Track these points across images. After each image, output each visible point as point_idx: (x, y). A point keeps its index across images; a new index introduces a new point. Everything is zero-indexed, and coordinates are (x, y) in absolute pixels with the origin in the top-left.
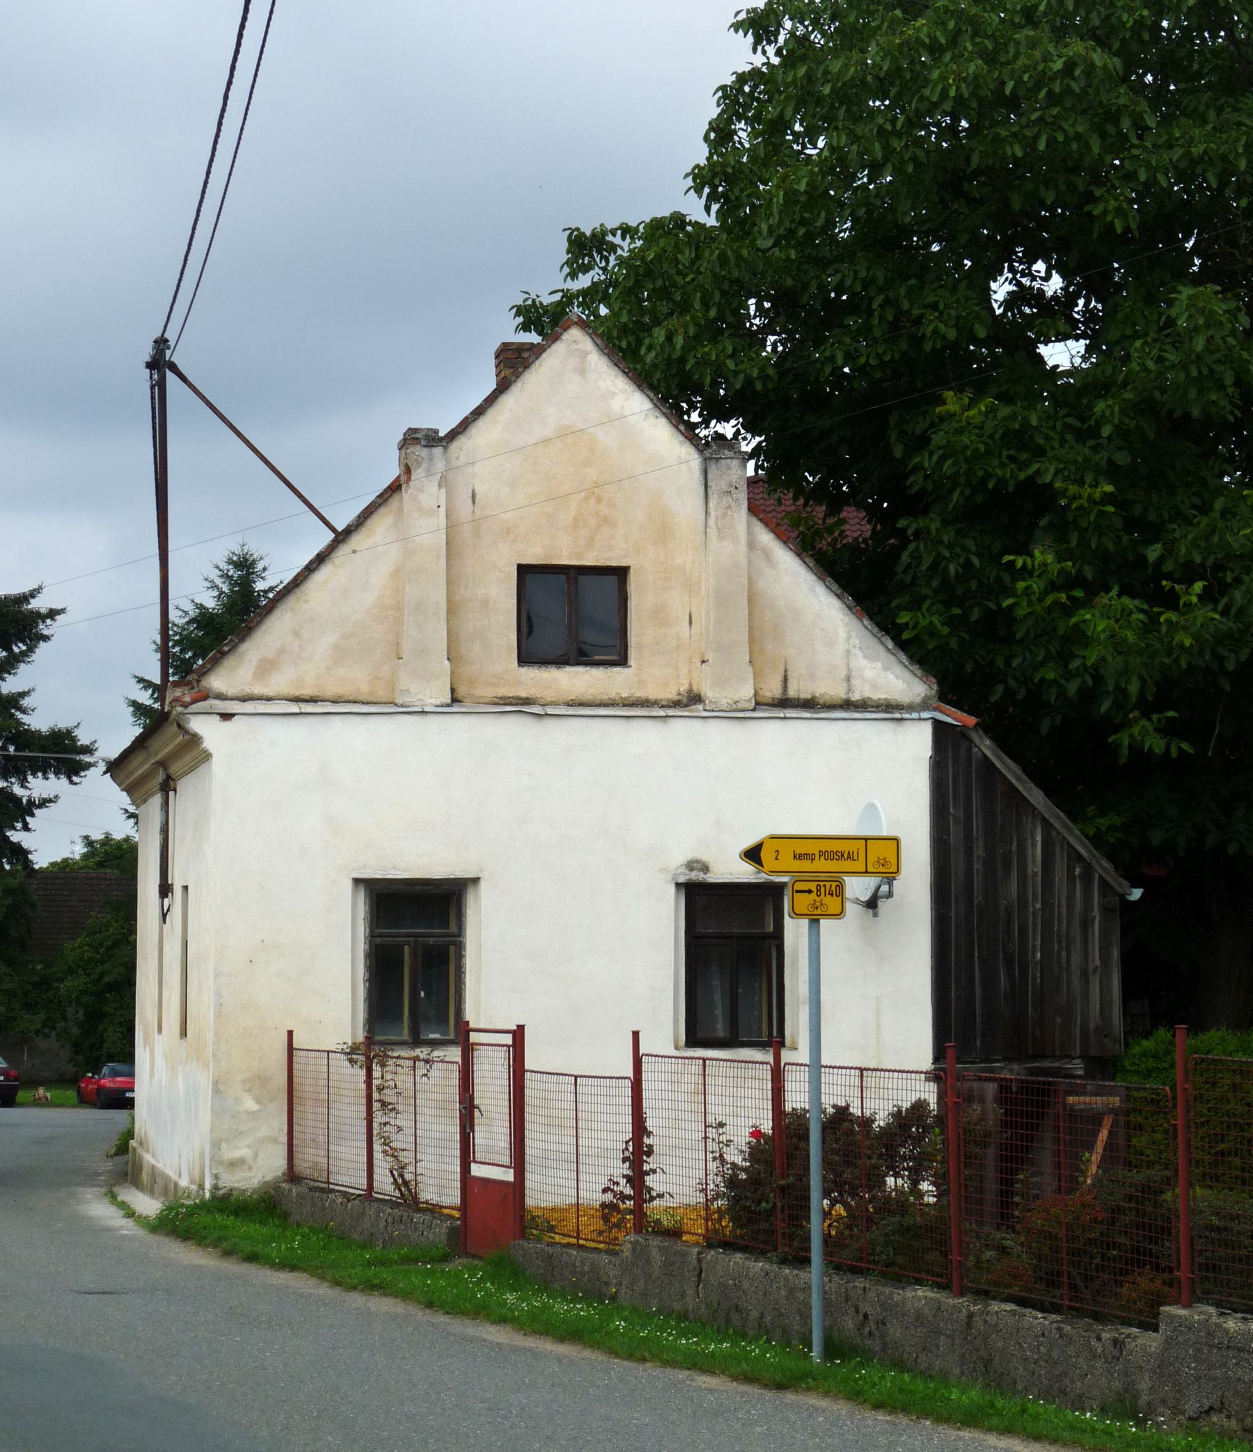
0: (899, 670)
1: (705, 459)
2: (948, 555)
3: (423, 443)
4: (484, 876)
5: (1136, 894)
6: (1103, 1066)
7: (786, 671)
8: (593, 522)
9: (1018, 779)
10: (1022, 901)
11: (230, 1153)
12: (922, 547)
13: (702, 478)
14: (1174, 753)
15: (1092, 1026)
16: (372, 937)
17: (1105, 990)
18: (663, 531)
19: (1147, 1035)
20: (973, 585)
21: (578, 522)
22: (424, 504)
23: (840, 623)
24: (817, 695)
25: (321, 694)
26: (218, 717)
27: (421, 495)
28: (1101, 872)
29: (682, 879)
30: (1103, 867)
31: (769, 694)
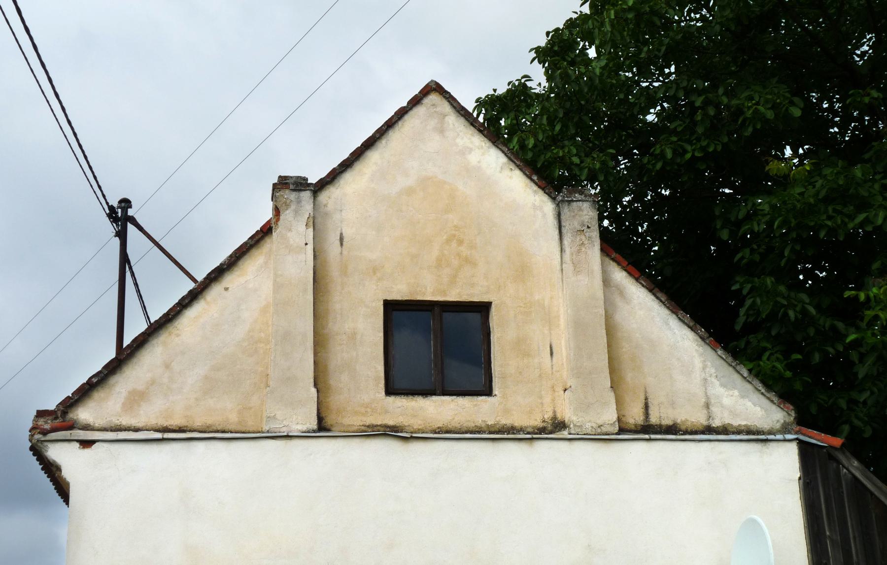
1: (558, 205)
2: (786, 303)
3: (292, 187)
7: (646, 399)
8: (455, 262)
12: (758, 301)
13: (556, 223)
18: (522, 270)
20: (812, 331)
21: (440, 263)
22: (292, 242)
23: (695, 354)
24: (679, 421)
26: (77, 445)
27: (289, 234)
31: (631, 421)
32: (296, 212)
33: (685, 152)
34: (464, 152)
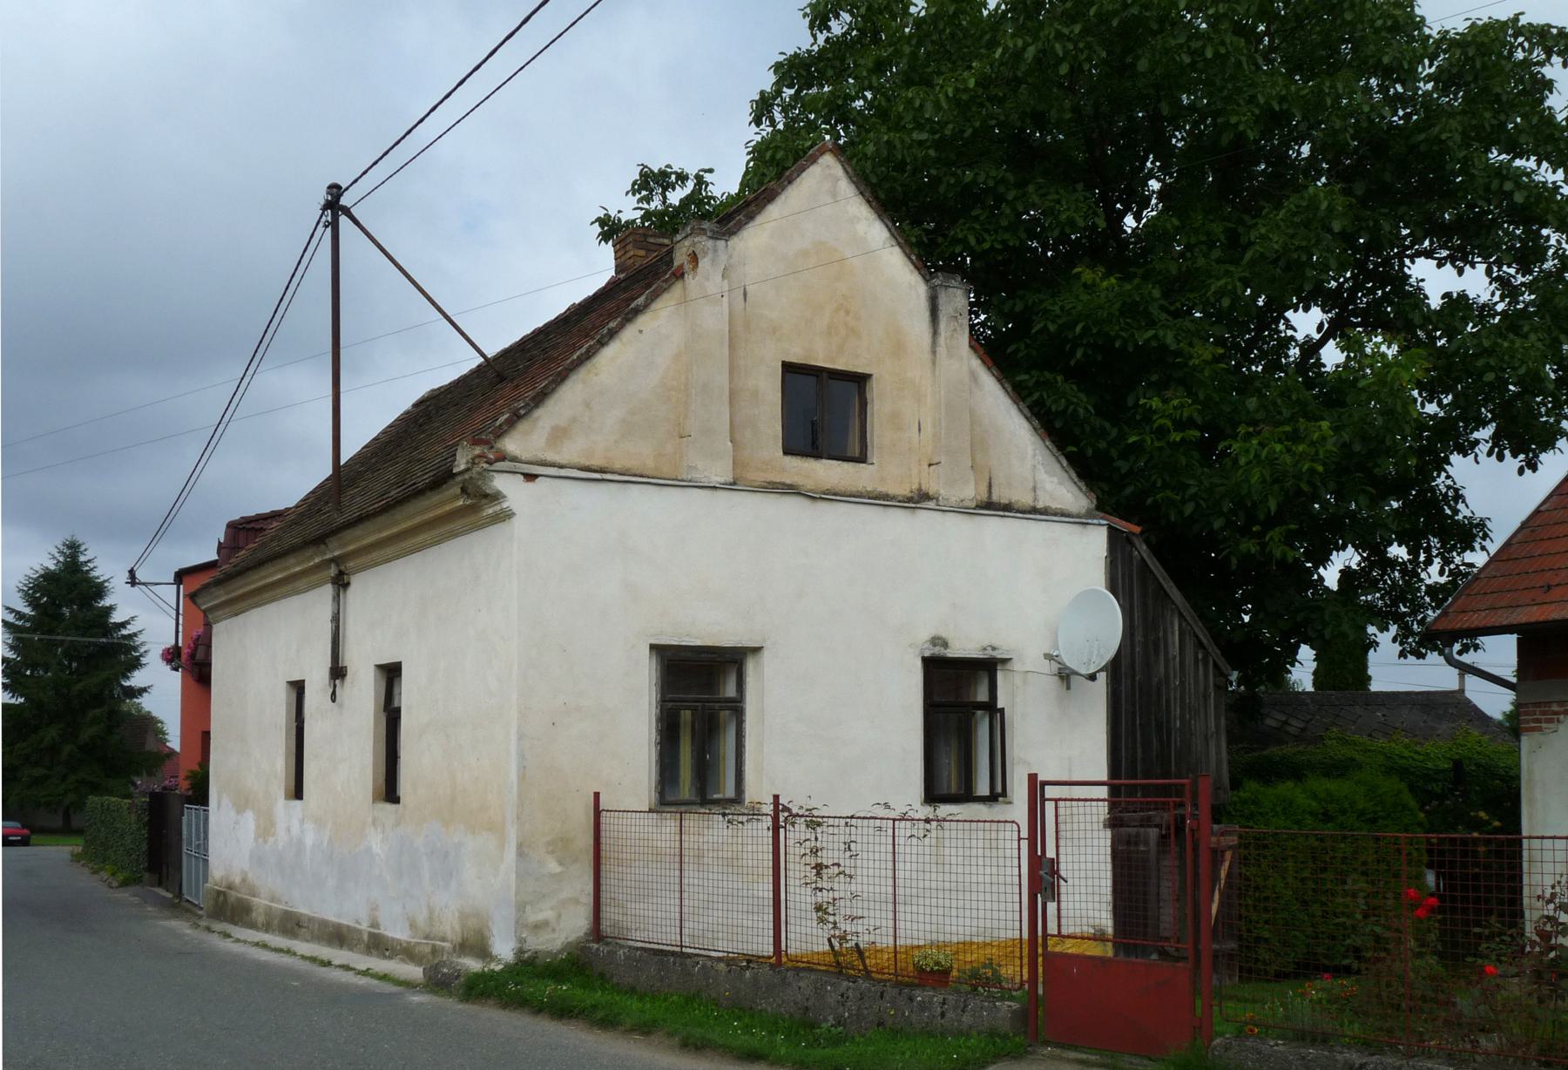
11: (534, 917)
16: (663, 701)
18: (898, 348)
29: (927, 654)
30: (1215, 652)
32: (713, 261)
33: (985, 240)
34: (861, 228)
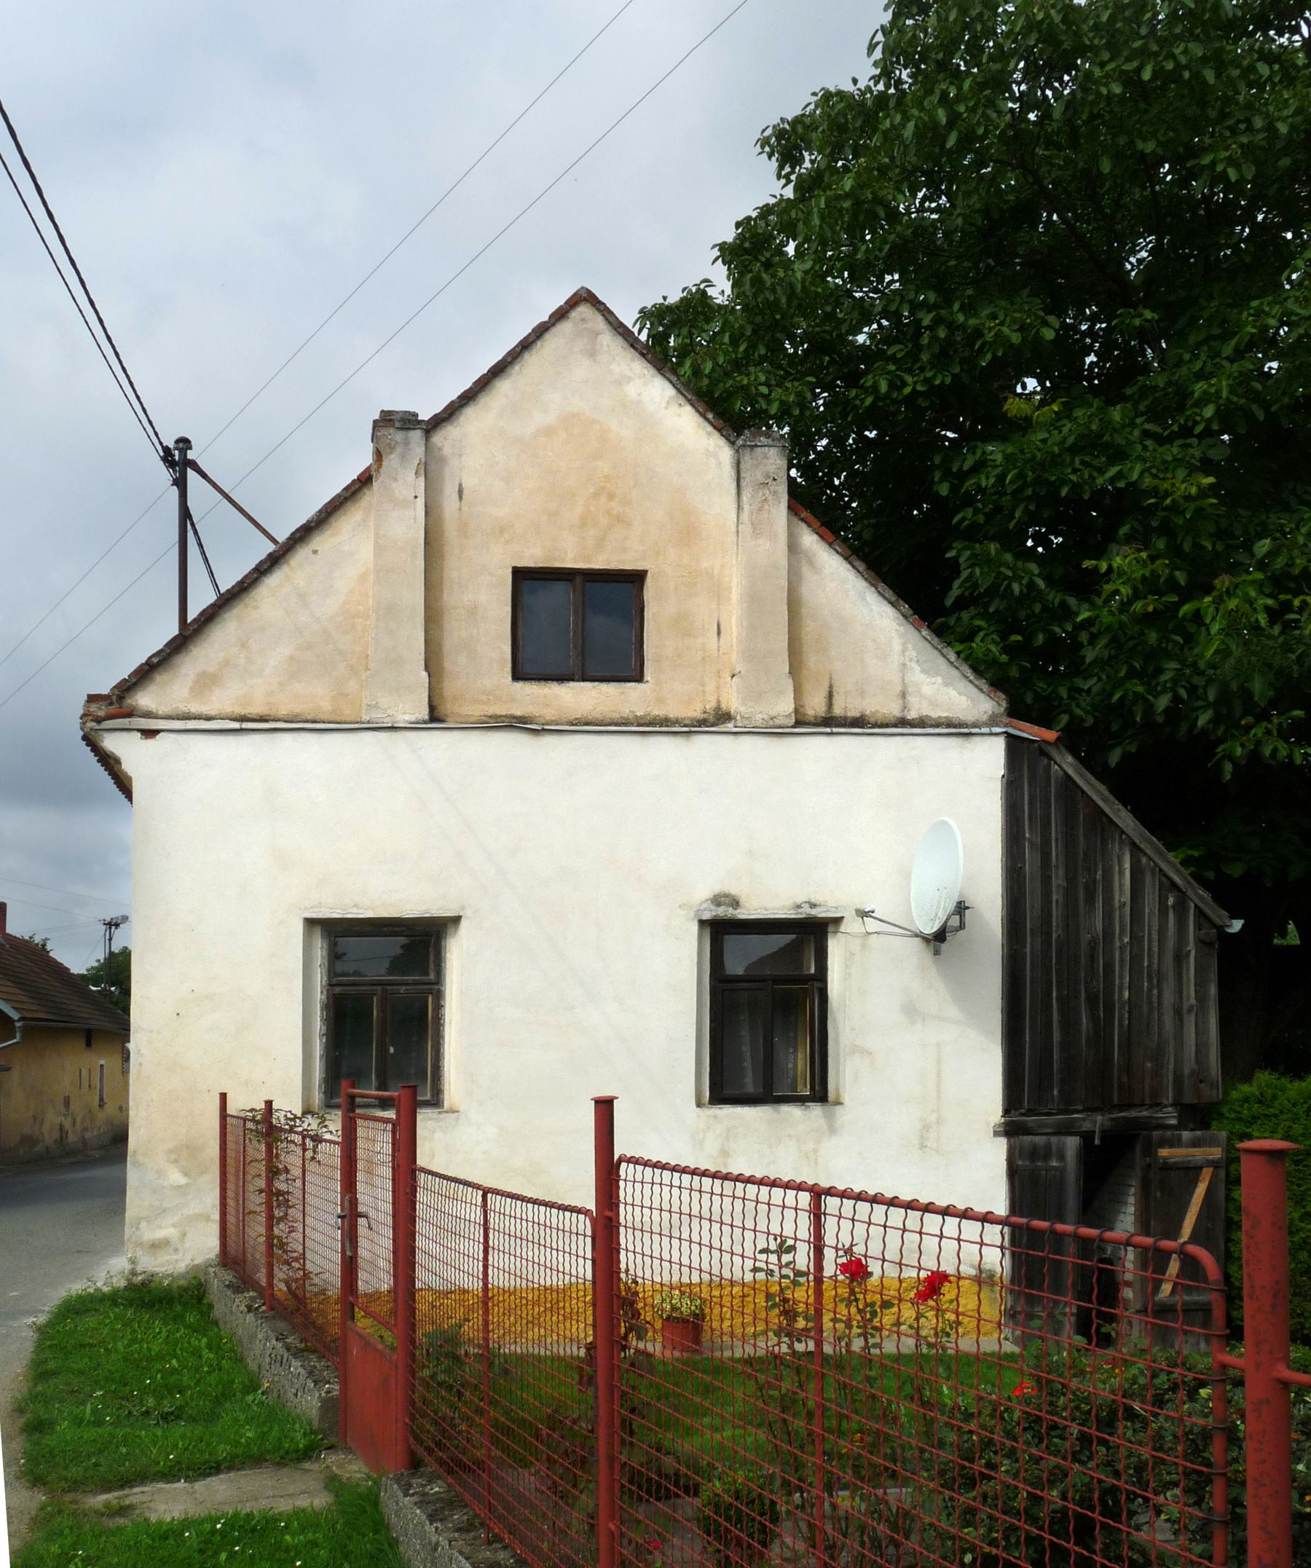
0: (963, 685)
1: (737, 451)
3: (397, 424)
4: (467, 914)
5: (1237, 925)
6: (1199, 1116)
7: (831, 687)
9: (1105, 800)
10: (1108, 934)
13: (733, 473)
14: (1298, 760)
15: (1186, 1071)
17: (1201, 1032)
18: (687, 530)
19: (1247, 1078)
21: (584, 523)
23: (894, 634)
25: (273, 713)
26: (139, 735)
27: (394, 485)
28: (1197, 901)
29: (707, 916)
30: (1200, 896)
33: (904, 384)
